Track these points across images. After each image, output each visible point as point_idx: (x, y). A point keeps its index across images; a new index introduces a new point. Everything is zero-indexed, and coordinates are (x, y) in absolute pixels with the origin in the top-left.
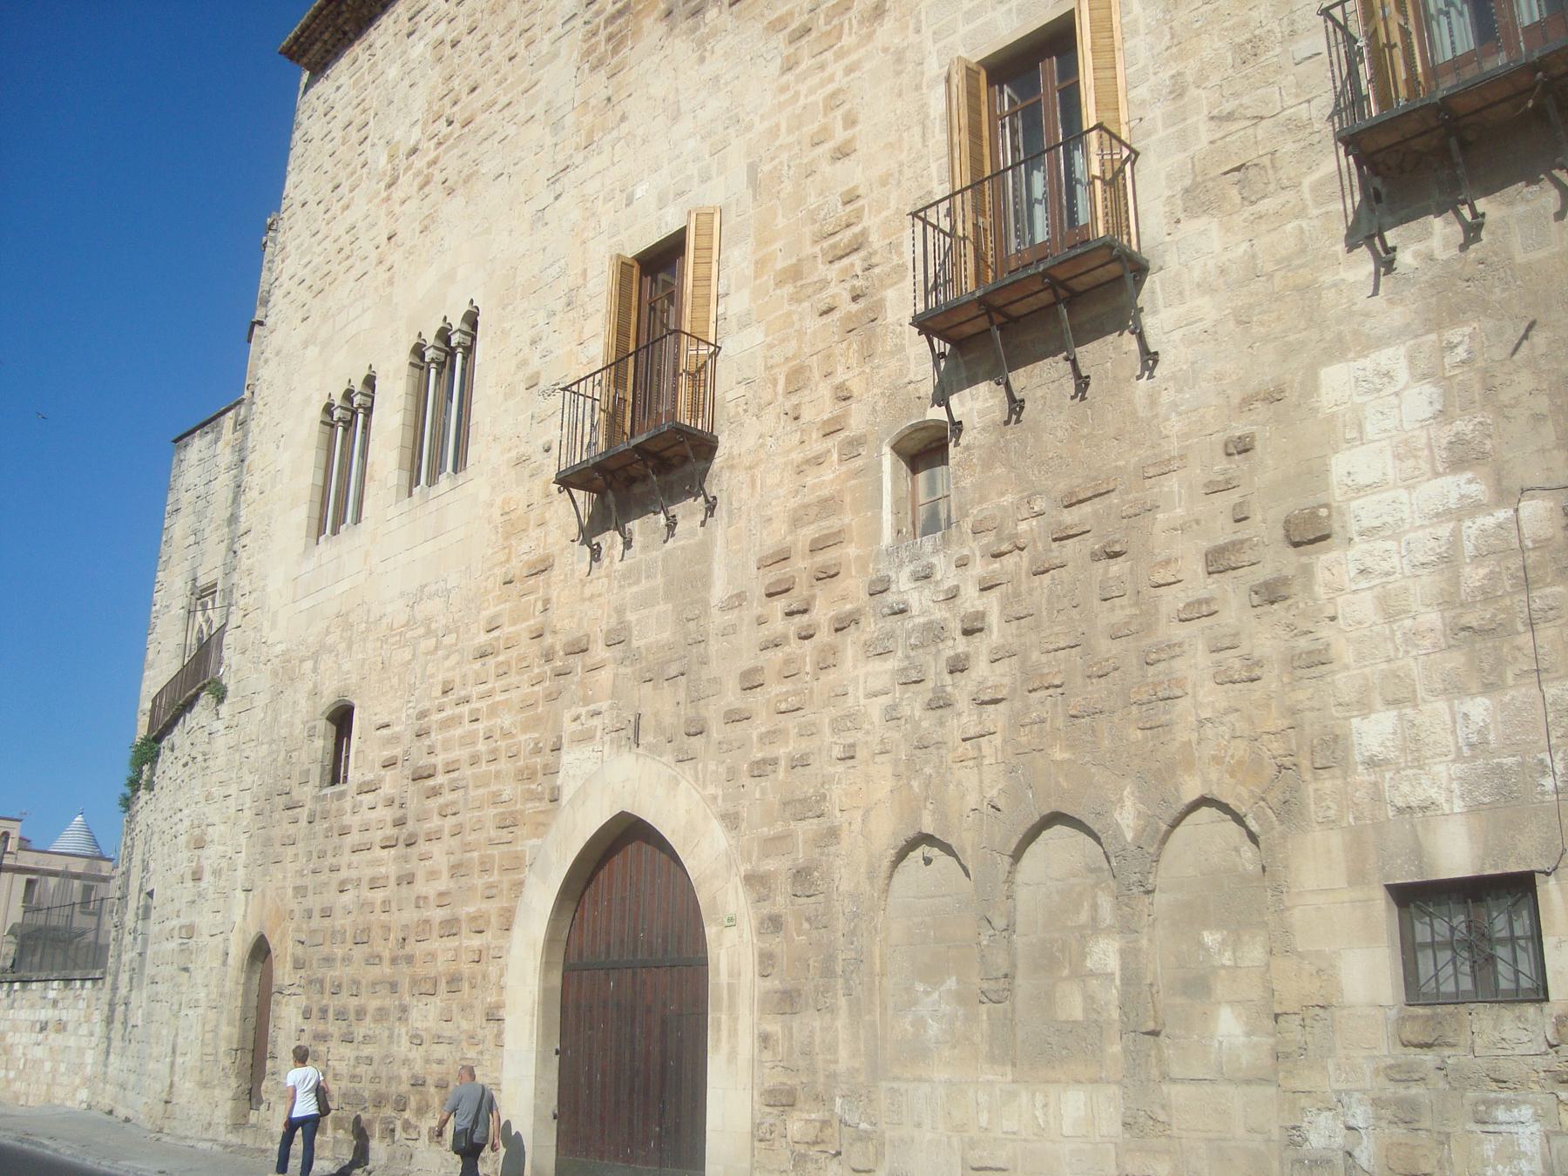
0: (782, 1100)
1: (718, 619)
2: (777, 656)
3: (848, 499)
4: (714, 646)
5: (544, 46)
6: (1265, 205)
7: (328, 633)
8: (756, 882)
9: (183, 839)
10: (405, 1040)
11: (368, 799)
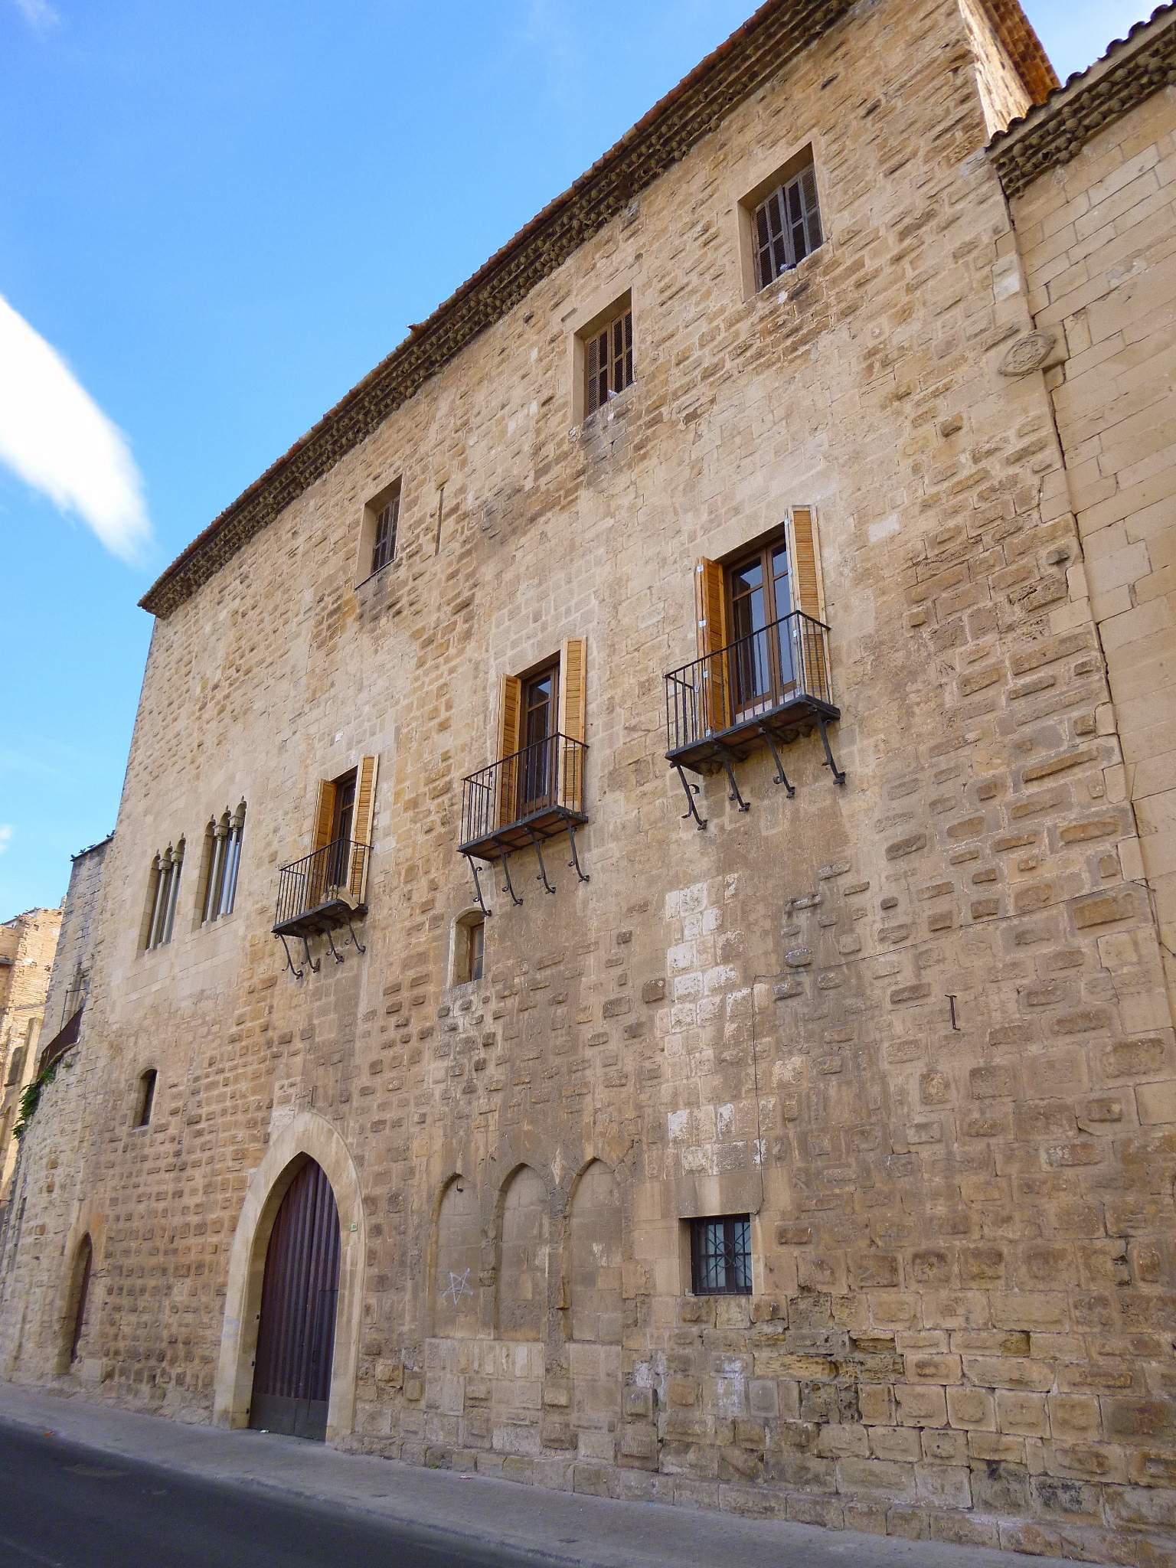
0: (374, 1352)
1: (362, 1027)
2: (391, 1053)
3: (432, 954)
4: (358, 1044)
5: (293, 626)
6: (648, 787)
7: (145, 1018)
8: (369, 1201)
9: (45, 1161)
10: (167, 1312)
11: (160, 1136)
